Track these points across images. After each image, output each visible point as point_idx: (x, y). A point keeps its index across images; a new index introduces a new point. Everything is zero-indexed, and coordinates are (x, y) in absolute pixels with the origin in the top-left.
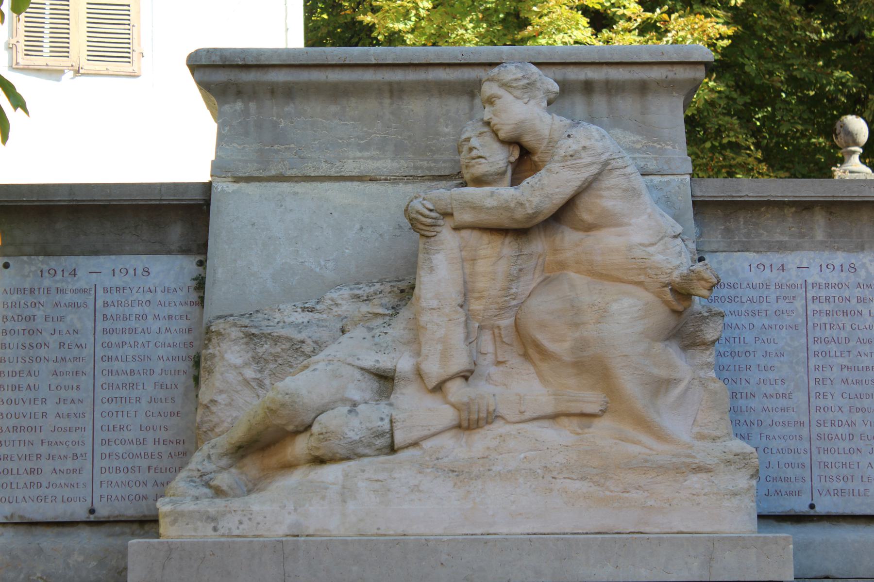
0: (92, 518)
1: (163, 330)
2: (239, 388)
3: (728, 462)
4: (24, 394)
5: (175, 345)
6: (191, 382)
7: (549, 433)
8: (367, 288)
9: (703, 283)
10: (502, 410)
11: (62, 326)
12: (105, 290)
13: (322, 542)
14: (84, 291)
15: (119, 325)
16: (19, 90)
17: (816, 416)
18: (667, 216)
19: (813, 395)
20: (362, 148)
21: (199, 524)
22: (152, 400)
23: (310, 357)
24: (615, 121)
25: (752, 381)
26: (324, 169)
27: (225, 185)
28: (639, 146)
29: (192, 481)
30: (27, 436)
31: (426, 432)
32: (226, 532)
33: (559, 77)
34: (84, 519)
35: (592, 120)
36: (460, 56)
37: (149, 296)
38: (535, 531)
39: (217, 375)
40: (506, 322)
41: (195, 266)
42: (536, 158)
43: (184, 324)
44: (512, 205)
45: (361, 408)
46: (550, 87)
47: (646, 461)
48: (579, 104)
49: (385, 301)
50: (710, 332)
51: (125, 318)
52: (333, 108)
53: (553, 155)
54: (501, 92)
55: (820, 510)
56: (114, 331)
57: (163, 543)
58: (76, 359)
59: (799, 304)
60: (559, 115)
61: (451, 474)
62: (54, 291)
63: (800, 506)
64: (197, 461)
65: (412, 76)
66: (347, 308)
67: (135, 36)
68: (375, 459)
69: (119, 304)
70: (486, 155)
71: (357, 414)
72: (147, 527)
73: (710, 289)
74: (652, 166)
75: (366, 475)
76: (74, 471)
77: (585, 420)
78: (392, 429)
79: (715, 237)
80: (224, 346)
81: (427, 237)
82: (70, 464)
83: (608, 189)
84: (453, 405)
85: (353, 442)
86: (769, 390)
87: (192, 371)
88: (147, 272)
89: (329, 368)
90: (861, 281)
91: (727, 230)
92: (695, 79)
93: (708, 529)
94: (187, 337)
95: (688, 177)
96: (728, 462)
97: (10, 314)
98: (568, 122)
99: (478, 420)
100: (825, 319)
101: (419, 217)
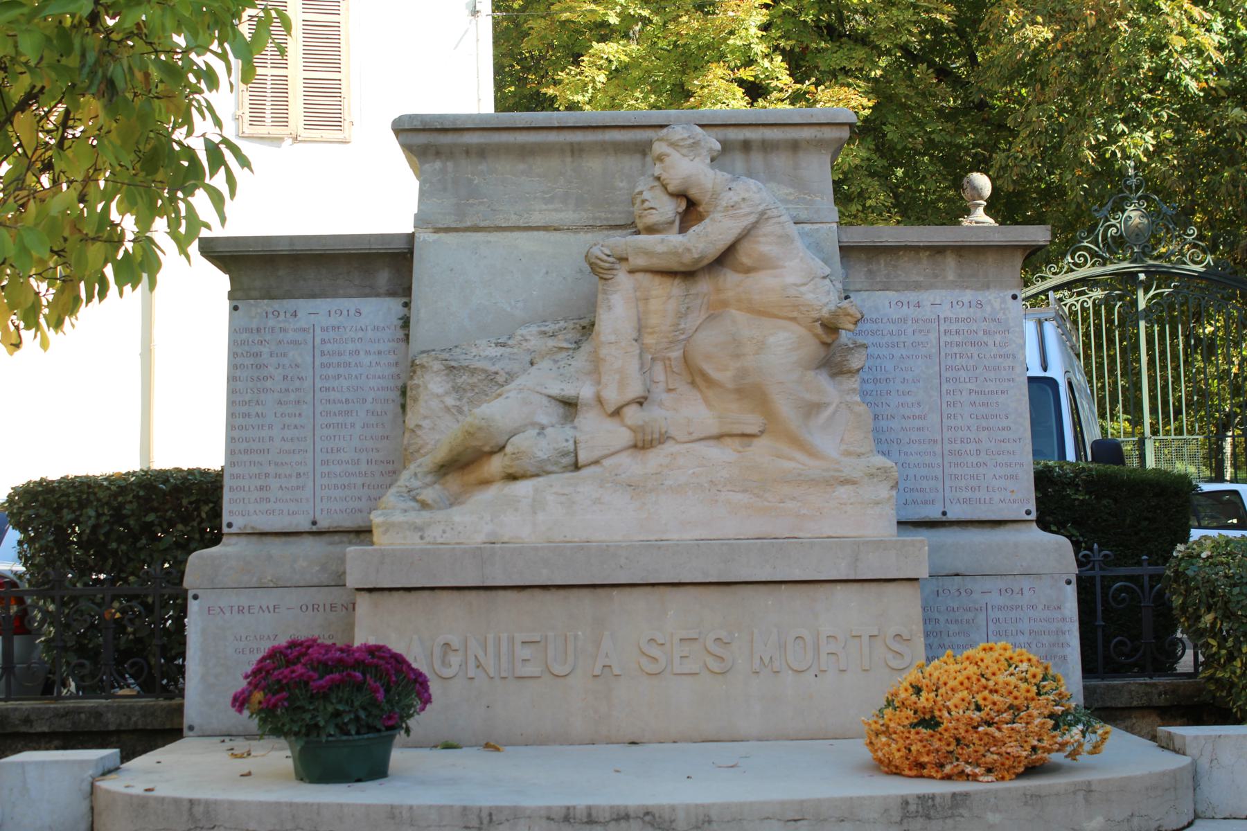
0: (314, 529)
1: (374, 364)
3: (872, 475)
5: (384, 377)
6: (399, 410)
7: (714, 452)
9: (849, 318)
11: (285, 361)
12: (322, 329)
14: (304, 330)
15: (335, 360)
17: (947, 435)
18: (817, 259)
19: (945, 416)
20: (547, 201)
23: (503, 386)
24: (771, 176)
26: (514, 220)
28: (791, 198)
30: (256, 458)
31: (607, 452)
33: (721, 137)
34: (307, 530)
35: (750, 175)
36: (633, 120)
37: (360, 334)
38: (703, 537)
40: (676, 354)
42: (701, 209)
44: (680, 250)
45: (549, 431)
46: (713, 146)
47: (800, 475)
48: (739, 161)
49: (569, 336)
50: (855, 362)
51: (340, 354)
52: (521, 166)
53: (716, 206)
55: (951, 516)
56: (330, 365)
57: (375, 550)
58: (298, 390)
59: (933, 336)
60: (721, 170)
61: (628, 488)
62: (277, 330)
63: (934, 513)
64: (405, 478)
65: (590, 137)
66: (535, 343)
69: (335, 341)
72: (362, 537)
73: (855, 324)
74: (803, 215)
76: (298, 488)
77: (746, 440)
79: (859, 276)
80: (427, 377)
81: (606, 279)
82: (294, 482)
83: (765, 235)
84: (630, 428)
85: (542, 461)
86: (907, 412)
87: (399, 400)
91: (870, 272)
93: (856, 534)
94: (394, 370)
95: (835, 225)
96: (872, 475)
98: (729, 176)
99: (652, 441)
100: (955, 350)
101: (598, 262)
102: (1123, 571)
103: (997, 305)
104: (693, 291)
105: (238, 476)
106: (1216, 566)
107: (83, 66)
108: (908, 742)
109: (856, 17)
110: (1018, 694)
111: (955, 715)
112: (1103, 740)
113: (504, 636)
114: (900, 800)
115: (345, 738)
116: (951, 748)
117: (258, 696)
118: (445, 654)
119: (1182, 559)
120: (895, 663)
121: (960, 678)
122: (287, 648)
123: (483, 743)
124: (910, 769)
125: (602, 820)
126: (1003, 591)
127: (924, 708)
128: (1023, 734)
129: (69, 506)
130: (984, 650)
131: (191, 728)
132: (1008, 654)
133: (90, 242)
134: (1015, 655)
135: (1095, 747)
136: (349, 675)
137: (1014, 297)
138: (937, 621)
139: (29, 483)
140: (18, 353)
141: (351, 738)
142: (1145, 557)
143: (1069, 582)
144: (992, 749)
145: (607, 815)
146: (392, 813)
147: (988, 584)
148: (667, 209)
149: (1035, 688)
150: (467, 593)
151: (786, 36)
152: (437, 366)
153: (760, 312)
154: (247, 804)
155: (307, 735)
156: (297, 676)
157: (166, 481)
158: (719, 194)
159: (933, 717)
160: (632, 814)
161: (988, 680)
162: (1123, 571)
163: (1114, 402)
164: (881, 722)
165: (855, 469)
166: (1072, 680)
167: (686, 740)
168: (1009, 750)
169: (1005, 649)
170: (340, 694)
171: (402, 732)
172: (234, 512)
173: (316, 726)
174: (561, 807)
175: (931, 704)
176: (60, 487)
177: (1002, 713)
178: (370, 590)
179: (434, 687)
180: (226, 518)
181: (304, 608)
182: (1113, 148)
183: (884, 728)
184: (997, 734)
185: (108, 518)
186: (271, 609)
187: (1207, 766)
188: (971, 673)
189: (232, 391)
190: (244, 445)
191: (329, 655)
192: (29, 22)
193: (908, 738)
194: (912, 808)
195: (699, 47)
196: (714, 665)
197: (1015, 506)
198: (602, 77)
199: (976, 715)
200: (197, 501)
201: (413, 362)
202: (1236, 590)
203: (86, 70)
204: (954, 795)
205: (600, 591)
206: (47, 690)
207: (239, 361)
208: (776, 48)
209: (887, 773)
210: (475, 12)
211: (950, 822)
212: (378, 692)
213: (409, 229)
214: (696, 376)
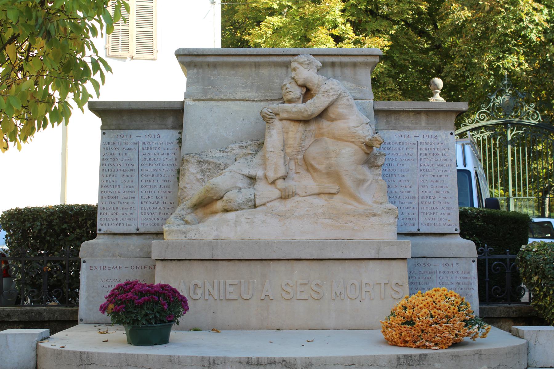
0: (138, 232)
1: (165, 159)
2: (195, 182)
3: (386, 212)
5: (170, 165)
6: (176, 180)
7: (317, 201)
8: (245, 143)
10: (298, 192)
11: (126, 157)
14: (135, 143)
15: (148, 157)
17: (421, 195)
19: (420, 186)
21: (179, 235)
22: (161, 187)
24: (344, 78)
25: (396, 181)
26: (229, 96)
28: (353, 88)
30: (112, 200)
31: (268, 200)
33: (322, 60)
35: (334, 77)
37: (159, 146)
39: (186, 177)
40: (300, 157)
42: (312, 92)
43: (173, 157)
44: (303, 111)
45: (243, 190)
47: (354, 212)
48: (329, 71)
49: (252, 148)
50: (380, 161)
51: (150, 154)
52: (233, 72)
53: (319, 91)
54: (299, 66)
55: (422, 231)
58: (131, 170)
59: (415, 151)
62: (122, 143)
63: (414, 230)
64: (178, 210)
65: (263, 59)
66: (237, 151)
69: (148, 149)
70: (293, 91)
71: (241, 192)
74: (358, 96)
76: (131, 214)
77: (331, 196)
78: (255, 199)
79: (382, 124)
80: (189, 165)
82: (129, 211)
83: (341, 105)
84: (279, 189)
86: (403, 184)
87: (176, 175)
89: (230, 174)
90: (439, 142)
91: (387, 122)
94: (174, 162)
95: (372, 100)
96: (386, 212)
98: (325, 78)
99: (289, 195)
100: (425, 157)
101: (266, 115)
102: (498, 257)
103: (444, 137)
105: (104, 208)
106: (539, 255)
108: (400, 331)
110: (450, 310)
111: (422, 319)
112: (487, 331)
113: (221, 282)
114: (396, 357)
115: (150, 325)
116: (419, 334)
117: (111, 306)
118: (195, 289)
119: (524, 252)
121: (424, 303)
122: (125, 285)
124: (401, 343)
125: (264, 364)
126: (444, 265)
127: (408, 316)
128: (452, 328)
131: (81, 320)
132: (446, 293)
134: (449, 293)
135: (483, 335)
136: (152, 297)
138: (415, 277)
140: (7, 152)
141: (152, 326)
143: (474, 261)
144: (437, 335)
145: (266, 361)
146: (170, 359)
147: (438, 261)
148: (297, 92)
149: (457, 308)
150: (205, 262)
151: (352, 15)
153: (338, 139)
155: (133, 324)
156: (129, 298)
157: (72, 210)
159: (412, 320)
160: (277, 361)
161: (436, 304)
162: (498, 257)
164: (389, 322)
166: (474, 305)
167: (302, 329)
168: (445, 335)
169: (444, 291)
170: (148, 306)
171: (175, 323)
172: (102, 224)
173: (137, 320)
174: (245, 358)
175: (411, 314)
177: (443, 319)
178: (162, 260)
179: (190, 304)
180: (98, 227)
181: (133, 267)
182: (498, 64)
183: (390, 325)
184: (440, 328)
186: (118, 268)
188: (429, 301)
189: (102, 170)
191: (143, 289)
193: (400, 329)
194: (402, 360)
195: (313, 20)
196: (315, 296)
197: (450, 227)
198: (270, 32)
199: (431, 320)
200: (86, 219)
202: (548, 266)
203: (38, 26)
204: (420, 355)
205: (264, 262)
207: (105, 157)
208: (348, 20)
209: (391, 345)
210: (213, 3)
214: (309, 167)
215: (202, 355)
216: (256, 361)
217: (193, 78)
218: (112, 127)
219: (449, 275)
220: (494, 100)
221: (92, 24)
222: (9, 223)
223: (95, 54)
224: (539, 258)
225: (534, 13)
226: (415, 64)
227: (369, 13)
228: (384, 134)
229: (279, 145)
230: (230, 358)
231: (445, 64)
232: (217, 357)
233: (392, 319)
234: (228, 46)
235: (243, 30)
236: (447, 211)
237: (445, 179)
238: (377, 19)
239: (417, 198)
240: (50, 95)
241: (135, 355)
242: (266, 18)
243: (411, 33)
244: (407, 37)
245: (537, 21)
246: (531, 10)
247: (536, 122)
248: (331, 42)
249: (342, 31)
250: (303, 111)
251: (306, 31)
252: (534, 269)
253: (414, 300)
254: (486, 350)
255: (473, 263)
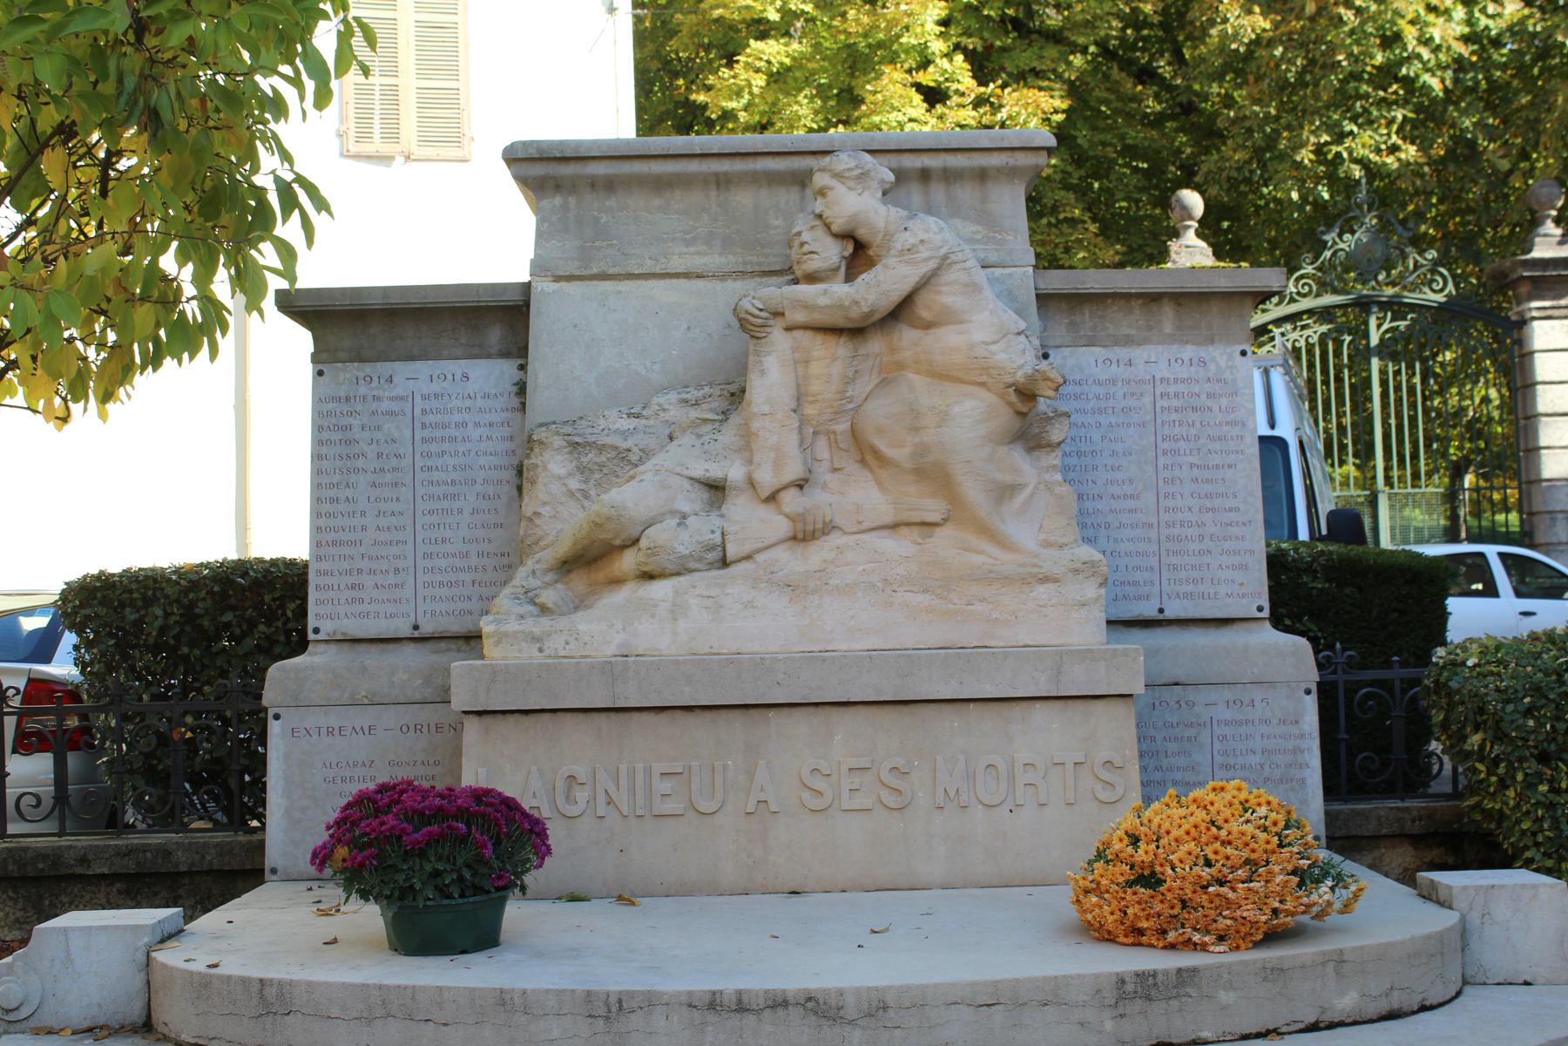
0: (416, 634)
1: (484, 438)
2: (563, 499)
3: (1076, 571)
4: (342, 507)
5: (496, 454)
6: (515, 492)
7: (888, 544)
8: (695, 392)
9: (1049, 383)
10: (839, 521)
11: (380, 435)
12: (423, 397)
13: (653, 662)
14: (402, 398)
15: (438, 433)
16: (323, 193)
17: (1164, 517)
18: (1010, 312)
19: (1161, 495)
20: (689, 243)
21: (524, 644)
22: (474, 512)
23: (636, 466)
24: (955, 212)
26: (649, 266)
27: (545, 285)
28: (979, 237)
29: (518, 599)
30: (346, 550)
31: (760, 545)
32: (553, 653)
33: (894, 165)
35: (930, 210)
36: (790, 145)
37: (468, 403)
39: (540, 486)
40: (842, 427)
41: (516, 371)
42: (871, 253)
43: (506, 432)
44: (847, 303)
45: (691, 520)
46: (885, 177)
47: (991, 572)
48: (915, 193)
49: (714, 405)
50: (1056, 433)
51: (445, 427)
52: (657, 202)
53: (889, 249)
54: (833, 183)
55: (1169, 614)
56: (432, 440)
58: (394, 469)
59: (1147, 400)
60: (895, 205)
61: (786, 589)
62: (370, 398)
63: (1148, 610)
64: (521, 577)
65: (739, 166)
66: (675, 413)
67: (465, 120)
68: (705, 573)
69: (438, 411)
70: (819, 250)
71: (686, 526)
73: (1056, 390)
74: (993, 257)
75: (698, 591)
76: (396, 586)
77: (926, 530)
79: (1060, 331)
80: (547, 455)
81: (758, 338)
83: (948, 284)
84: (787, 516)
85: (683, 557)
86: (1116, 490)
87: (515, 481)
88: (466, 377)
89: (658, 477)
90: (1210, 375)
91: (1072, 324)
92: (1037, 166)
93: (1055, 642)
94: (509, 445)
95: (1031, 269)
96: (1076, 571)
97: (326, 424)
98: (904, 213)
100: (1174, 416)
101: (749, 317)
102: (1370, 675)
103: (1223, 364)
104: (862, 351)
105: (326, 573)
106: (1485, 676)
107: (120, 94)
109: (1047, 10)
110: (1256, 846)
111: (1181, 872)
112: (1356, 896)
113: (639, 767)
114: (1114, 979)
115: (446, 902)
116: (1175, 911)
117: (342, 852)
118: (570, 788)
119: (1444, 667)
120: (1105, 796)
121: (1186, 827)
123: (616, 894)
124: (1126, 936)
125: (755, 1007)
126: (1231, 703)
128: (1262, 895)
129: (132, 603)
130: (1214, 789)
131: (274, 871)
132: (1243, 796)
133: (138, 304)
134: (1251, 797)
135: (1345, 906)
136: (449, 827)
137: (1244, 353)
138: (1153, 739)
139: (85, 577)
140: (67, 427)
142: (1396, 658)
143: (1308, 692)
144: (1224, 913)
145: (761, 1001)
146: (502, 999)
147: (1213, 694)
148: (831, 253)
149: (1276, 838)
150: (595, 715)
151: (967, 33)
152: (558, 442)
153: (942, 375)
154: (328, 984)
155: (401, 898)
156: (388, 830)
157: (245, 574)
158: (893, 235)
159: (1153, 874)
160: (792, 1001)
161: (1219, 828)
162: (1370, 675)
163: (1343, 447)
164: (1091, 878)
165: (1054, 561)
166: (1313, 806)
167: (857, 889)
168: (1245, 914)
169: (1239, 789)
170: (440, 851)
171: (517, 891)
172: (322, 615)
173: (412, 887)
174: (705, 992)
175: (1151, 857)
176: (121, 582)
177: (1237, 869)
178: (480, 713)
180: (312, 622)
181: (405, 729)
182: (1339, 149)
183: (1094, 886)
184: (1231, 895)
185: (178, 618)
186: (367, 732)
187: (1478, 922)
188: (1199, 819)
189: (317, 471)
190: (331, 536)
192: (49, 42)
193: (1123, 899)
194: (1130, 987)
195: (869, 46)
196: (891, 800)
197: (1244, 601)
198: (759, 81)
199: (1206, 873)
200: (282, 598)
201: (530, 436)
202: (1510, 708)
203: (123, 99)
204: (1179, 970)
205: (752, 712)
206: (114, 822)
207: (325, 435)
208: (957, 47)
209: (1098, 939)
210: (612, 10)
211: (1175, 1003)
212: (485, 846)
213: (525, 277)
214: (866, 454)
215: (588, 987)
216: (734, 1000)
217: (554, 218)
218: (342, 355)
219: (1243, 730)
220: (1335, 243)
221: (273, 88)
222: (84, 612)
223: (286, 165)
224: (1486, 687)
225: (1431, 18)
226: (1130, 151)
227: (1010, 27)
228: (1065, 358)
229: (785, 397)
230: (664, 994)
231: (1207, 151)
232: (627, 992)
233: (1101, 871)
234: (643, 135)
235: (692, 76)
236: (1236, 560)
237: (1229, 473)
238: (1031, 41)
239: (1155, 525)
240: (165, 278)
241: (406, 988)
242: (749, 46)
243: (1115, 73)
244: (1108, 85)
245: (1437, 41)
246: (1422, 12)
247: (1440, 298)
248: (914, 104)
249: (942, 75)
250: (847, 303)
251: (852, 75)
252: (1471, 716)
253: (1158, 818)
254: (1354, 949)
255: (1308, 697)
